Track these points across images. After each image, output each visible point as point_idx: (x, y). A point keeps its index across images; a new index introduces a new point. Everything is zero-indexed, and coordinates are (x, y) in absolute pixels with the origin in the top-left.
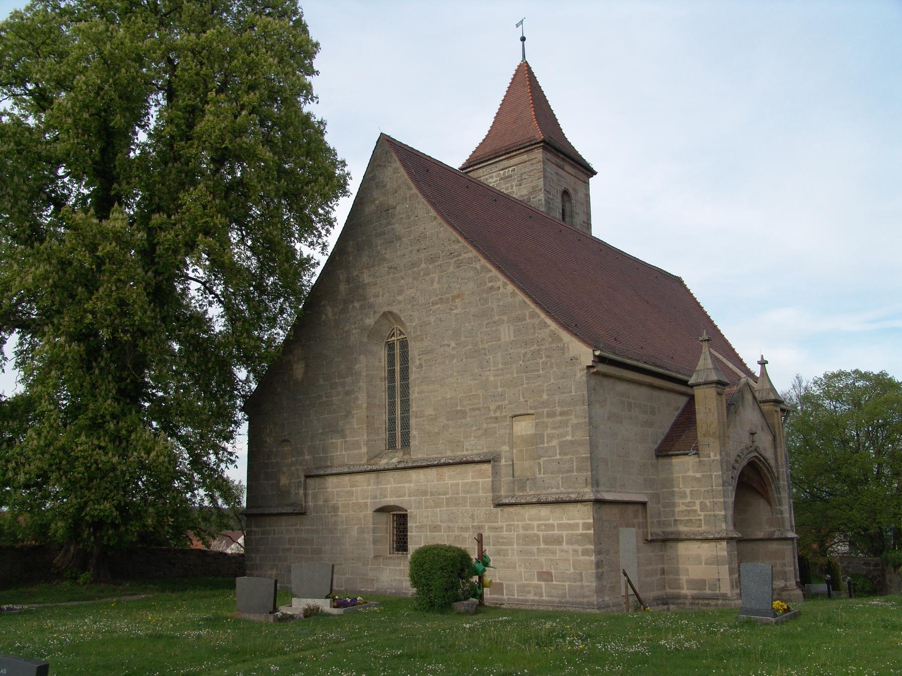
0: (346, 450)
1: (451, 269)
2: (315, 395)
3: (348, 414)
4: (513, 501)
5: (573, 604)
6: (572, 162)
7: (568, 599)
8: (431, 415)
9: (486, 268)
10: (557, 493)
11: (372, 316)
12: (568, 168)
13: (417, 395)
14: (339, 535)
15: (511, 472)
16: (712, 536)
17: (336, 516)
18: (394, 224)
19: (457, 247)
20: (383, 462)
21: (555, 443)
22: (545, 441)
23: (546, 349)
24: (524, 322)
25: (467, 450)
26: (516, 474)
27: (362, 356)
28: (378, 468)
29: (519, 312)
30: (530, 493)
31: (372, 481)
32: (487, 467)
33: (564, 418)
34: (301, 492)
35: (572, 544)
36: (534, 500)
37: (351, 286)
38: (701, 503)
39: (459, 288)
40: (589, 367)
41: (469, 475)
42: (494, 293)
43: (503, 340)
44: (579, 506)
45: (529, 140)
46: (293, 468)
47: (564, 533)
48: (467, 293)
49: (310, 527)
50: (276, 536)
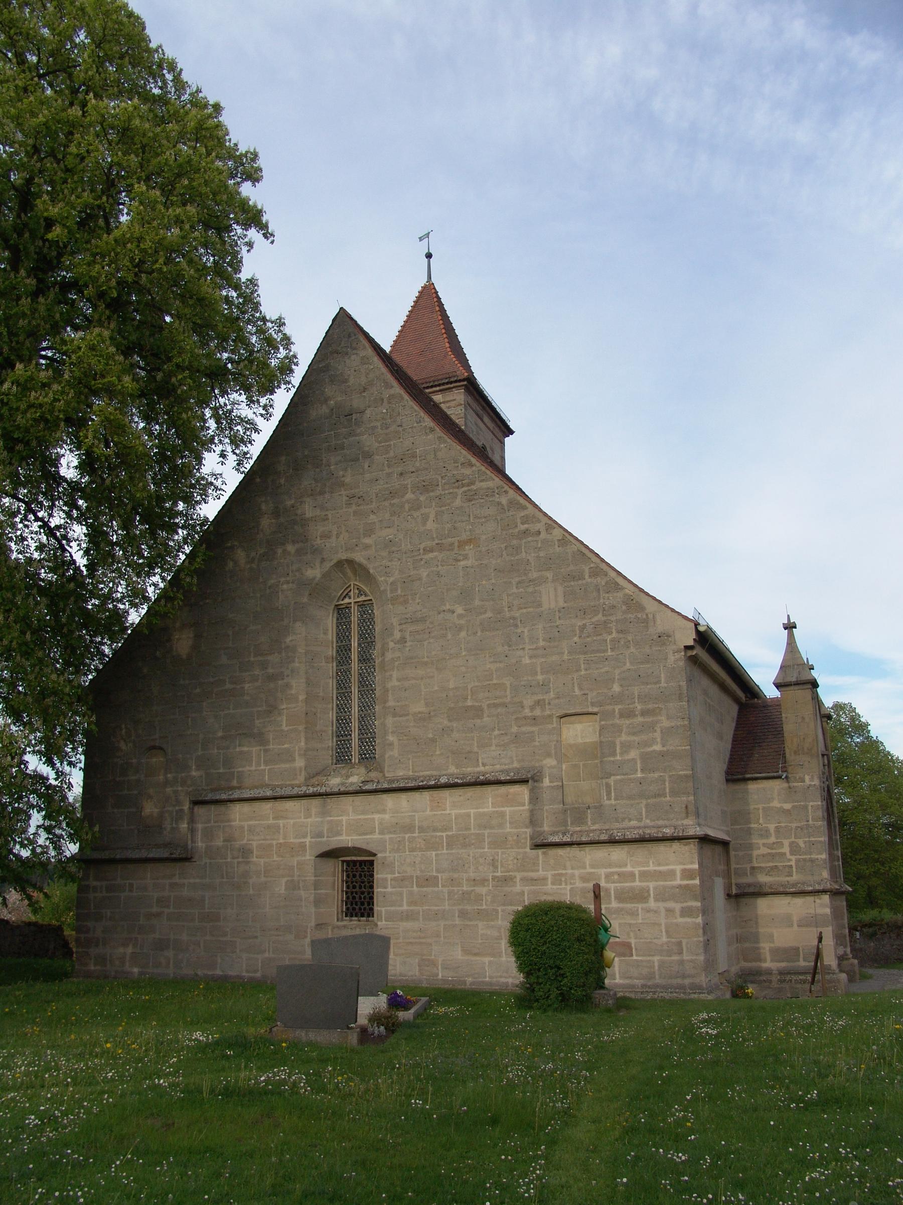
0: (266, 763)
1: (458, 502)
2: (212, 680)
3: (272, 709)
4: (567, 839)
5: (665, 988)
6: (492, 414)
7: (658, 980)
8: (419, 713)
9: (518, 503)
10: (639, 828)
13: (397, 684)
14: (251, 892)
16: (810, 888)
17: (249, 862)
19: (467, 471)
20: (334, 782)
21: (633, 754)
22: (618, 751)
23: (617, 621)
24: (580, 582)
25: (484, 765)
27: (298, 624)
28: (328, 790)
29: (572, 567)
30: (593, 828)
31: (314, 811)
32: (523, 792)
33: (649, 719)
34: (184, 826)
36: (604, 837)
37: (282, 520)
38: (791, 844)
39: (470, 530)
40: (687, 648)
41: (488, 800)
42: (530, 539)
43: (545, 606)
44: (676, 845)
45: (447, 376)
46: (169, 790)
47: (652, 885)
48: (484, 537)
49: (197, 880)
50: (134, 894)
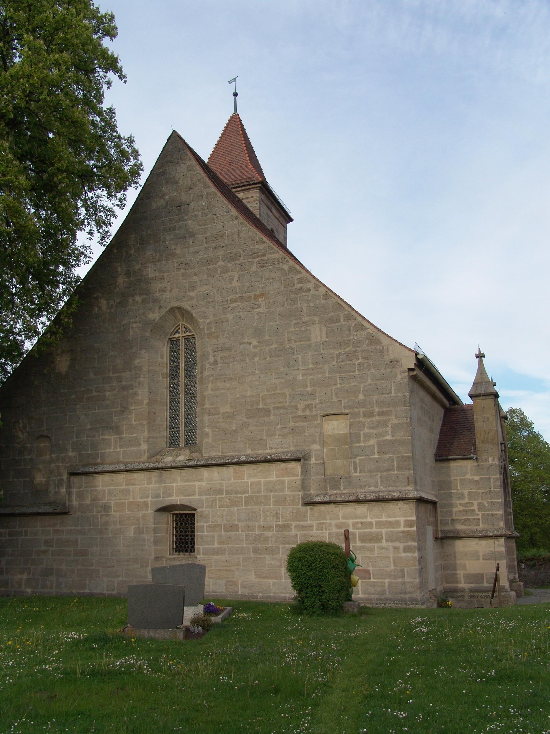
0: (121, 447)
1: (254, 268)
2: (83, 389)
3: (125, 410)
4: (326, 499)
5: (392, 600)
7: (388, 595)
8: (227, 412)
9: (296, 269)
10: (376, 492)
11: (157, 310)
12: (274, 211)
13: (211, 392)
14: (110, 535)
15: (322, 471)
16: (492, 534)
18: (186, 220)
19: (261, 247)
20: (168, 460)
21: (372, 442)
22: (362, 439)
23: (362, 351)
24: (337, 324)
25: (270, 448)
26: (328, 472)
27: (143, 351)
28: (164, 465)
29: (332, 314)
30: (344, 492)
31: (154, 480)
32: (297, 467)
33: (383, 418)
34: (63, 490)
35: (392, 541)
36: (352, 498)
37: (132, 279)
38: (479, 504)
39: (263, 288)
40: (410, 370)
42: (303, 294)
43: (314, 340)
44: (400, 504)
45: (248, 180)
46: (53, 465)
47: (384, 531)
48: (272, 292)
49: (73, 528)
